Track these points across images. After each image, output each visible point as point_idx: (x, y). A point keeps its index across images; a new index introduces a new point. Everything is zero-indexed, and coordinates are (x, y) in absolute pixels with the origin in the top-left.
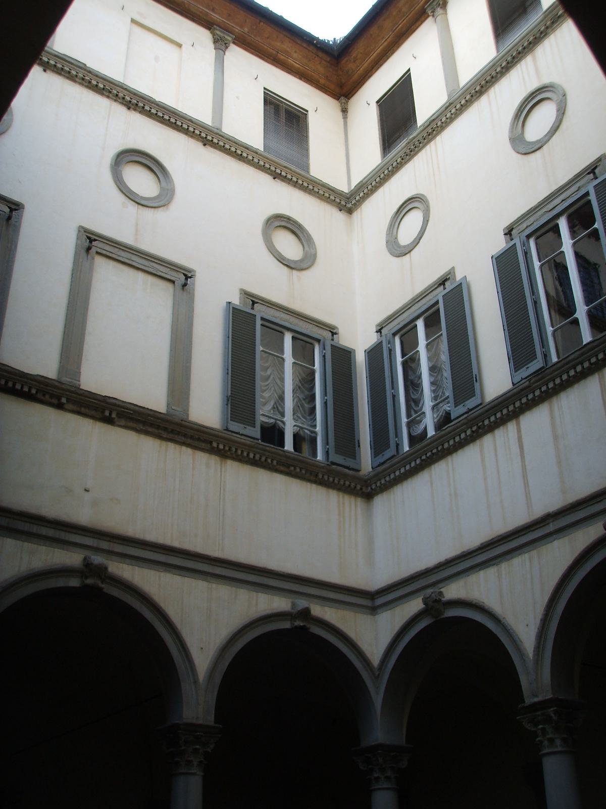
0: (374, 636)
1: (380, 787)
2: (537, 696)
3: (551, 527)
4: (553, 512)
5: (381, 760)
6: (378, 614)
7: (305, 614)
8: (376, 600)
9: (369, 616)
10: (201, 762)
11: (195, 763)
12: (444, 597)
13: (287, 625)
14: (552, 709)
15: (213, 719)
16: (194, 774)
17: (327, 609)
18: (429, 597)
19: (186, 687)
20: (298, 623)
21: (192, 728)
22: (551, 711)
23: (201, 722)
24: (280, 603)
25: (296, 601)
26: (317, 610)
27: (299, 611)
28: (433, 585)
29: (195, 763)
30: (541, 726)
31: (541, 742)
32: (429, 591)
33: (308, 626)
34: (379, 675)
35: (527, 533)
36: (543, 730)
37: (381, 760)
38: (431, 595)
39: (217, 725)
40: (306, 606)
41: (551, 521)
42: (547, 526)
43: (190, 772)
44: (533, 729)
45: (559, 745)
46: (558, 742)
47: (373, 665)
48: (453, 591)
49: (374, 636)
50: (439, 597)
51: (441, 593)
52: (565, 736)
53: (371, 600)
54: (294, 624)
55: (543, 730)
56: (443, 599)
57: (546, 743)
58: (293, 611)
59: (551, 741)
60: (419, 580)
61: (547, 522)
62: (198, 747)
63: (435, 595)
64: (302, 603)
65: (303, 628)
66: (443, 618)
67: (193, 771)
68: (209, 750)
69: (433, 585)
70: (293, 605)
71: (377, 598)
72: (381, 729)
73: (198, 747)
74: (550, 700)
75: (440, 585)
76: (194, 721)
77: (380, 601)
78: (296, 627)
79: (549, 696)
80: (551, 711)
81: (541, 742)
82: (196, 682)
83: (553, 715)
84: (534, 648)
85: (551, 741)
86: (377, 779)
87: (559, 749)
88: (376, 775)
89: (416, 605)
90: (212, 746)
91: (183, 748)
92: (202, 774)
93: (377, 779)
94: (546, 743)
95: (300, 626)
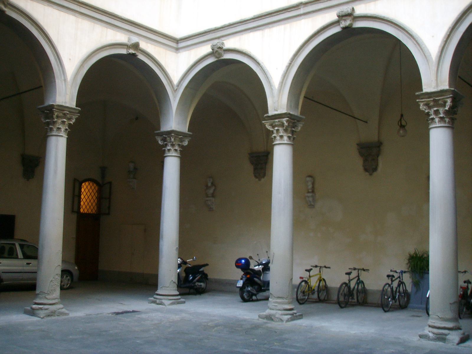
0: (176, 67)
1: (171, 155)
2: (277, 111)
3: (302, 11)
4: (304, 2)
5: (173, 140)
6: (180, 53)
7: (136, 46)
8: (179, 44)
9: (174, 54)
10: (66, 129)
11: (63, 130)
12: (224, 46)
13: (124, 51)
14: (285, 119)
15: (75, 104)
16: (62, 136)
17: (149, 45)
18: (215, 45)
19: (59, 83)
20: (132, 51)
21: (62, 108)
22: (284, 120)
23: (67, 105)
24: (121, 37)
25: (131, 37)
26: (144, 45)
27: (132, 44)
28: (219, 38)
29: (63, 130)
30: (276, 128)
31: (275, 137)
32: (215, 42)
33: (137, 54)
34: (177, 89)
35: (286, 12)
36: (278, 130)
37: (173, 140)
38: (217, 44)
39: (77, 108)
40: (138, 41)
41: (302, 7)
42: (299, 10)
43: (59, 134)
44: (271, 129)
45: (285, 140)
46: (285, 138)
47: (173, 83)
48: (230, 43)
49: (176, 67)
50: (222, 46)
51: (223, 44)
52: (290, 135)
53: (177, 43)
54: (128, 51)
55: (278, 130)
56: (224, 47)
57: (278, 138)
58: (129, 43)
59: (281, 137)
60: (209, 34)
61: (299, 7)
62: (65, 120)
63: (220, 44)
64: (135, 39)
65: (134, 55)
66: (223, 59)
67: (61, 134)
68: (72, 123)
69: (219, 38)
70: (129, 39)
71: (180, 43)
72: (175, 120)
73: (65, 120)
74: (285, 114)
75: (223, 39)
76: (64, 104)
77: (181, 45)
78: (130, 54)
79: (284, 111)
80: (284, 120)
81: (275, 137)
82: (65, 80)
83: (285, 122)
84: (280, 82)
85: (281, 137)
86: (169, 150)
87: (286, 142)
88: (169, 148)
89: (206, 49)
90: (74, 121)
91: (55, 120)
92: (67, 137)
93: (169, 150)
94: (278, 138)
95: (133, 53)
